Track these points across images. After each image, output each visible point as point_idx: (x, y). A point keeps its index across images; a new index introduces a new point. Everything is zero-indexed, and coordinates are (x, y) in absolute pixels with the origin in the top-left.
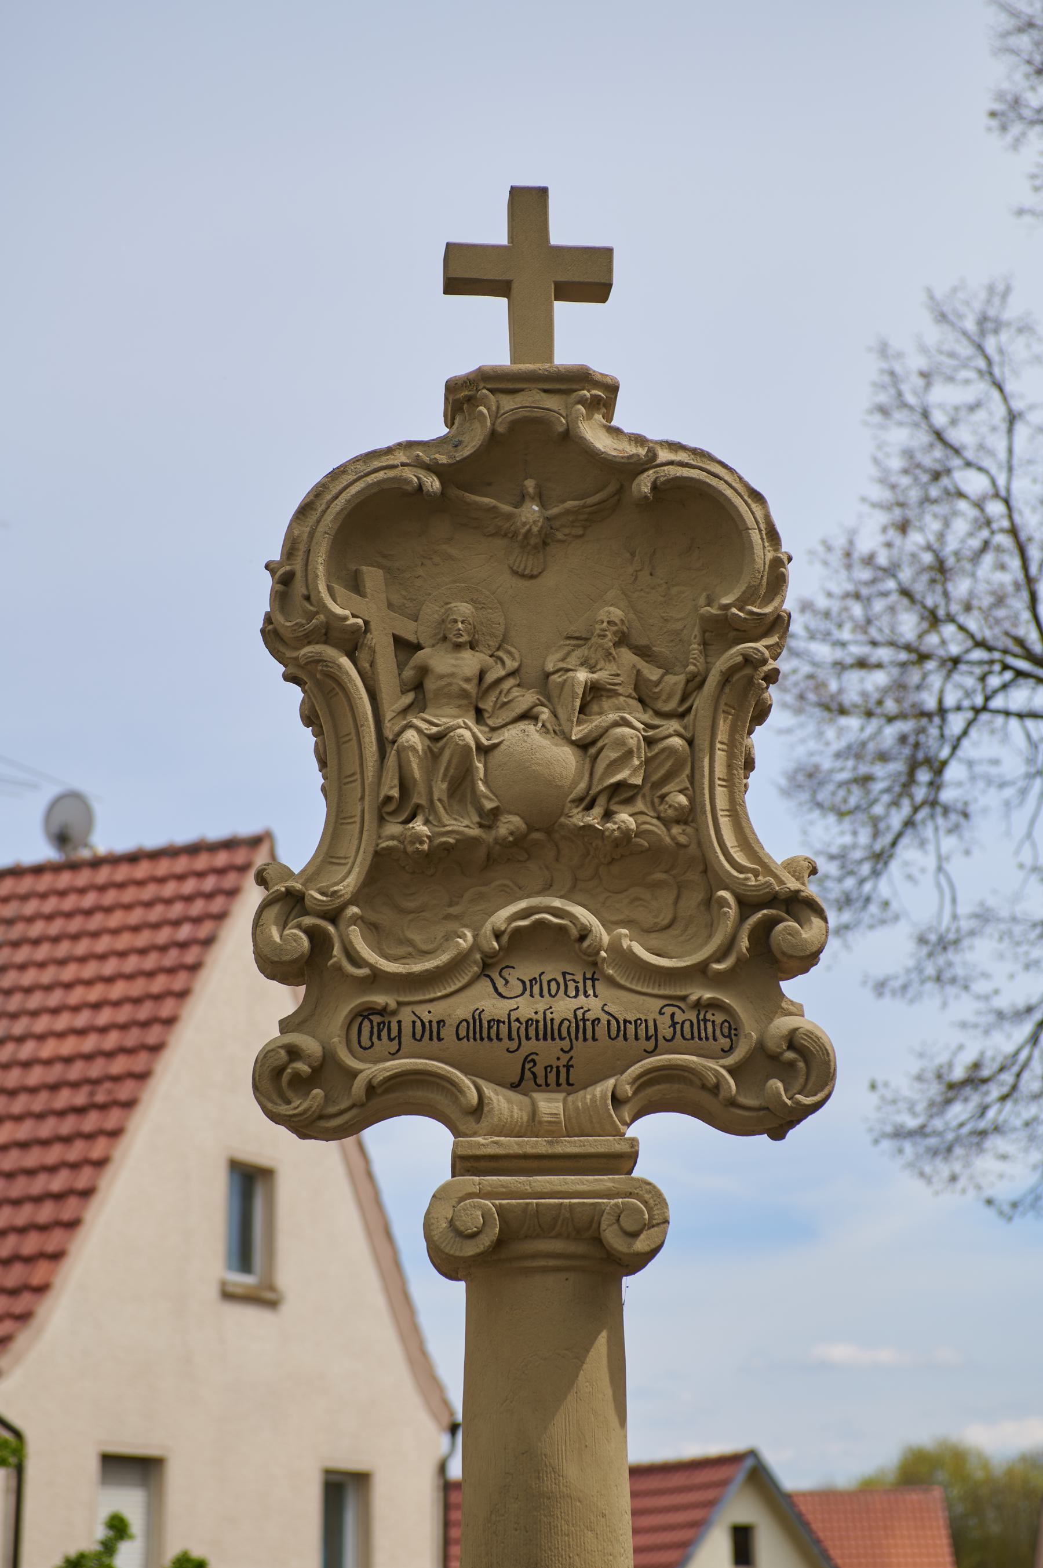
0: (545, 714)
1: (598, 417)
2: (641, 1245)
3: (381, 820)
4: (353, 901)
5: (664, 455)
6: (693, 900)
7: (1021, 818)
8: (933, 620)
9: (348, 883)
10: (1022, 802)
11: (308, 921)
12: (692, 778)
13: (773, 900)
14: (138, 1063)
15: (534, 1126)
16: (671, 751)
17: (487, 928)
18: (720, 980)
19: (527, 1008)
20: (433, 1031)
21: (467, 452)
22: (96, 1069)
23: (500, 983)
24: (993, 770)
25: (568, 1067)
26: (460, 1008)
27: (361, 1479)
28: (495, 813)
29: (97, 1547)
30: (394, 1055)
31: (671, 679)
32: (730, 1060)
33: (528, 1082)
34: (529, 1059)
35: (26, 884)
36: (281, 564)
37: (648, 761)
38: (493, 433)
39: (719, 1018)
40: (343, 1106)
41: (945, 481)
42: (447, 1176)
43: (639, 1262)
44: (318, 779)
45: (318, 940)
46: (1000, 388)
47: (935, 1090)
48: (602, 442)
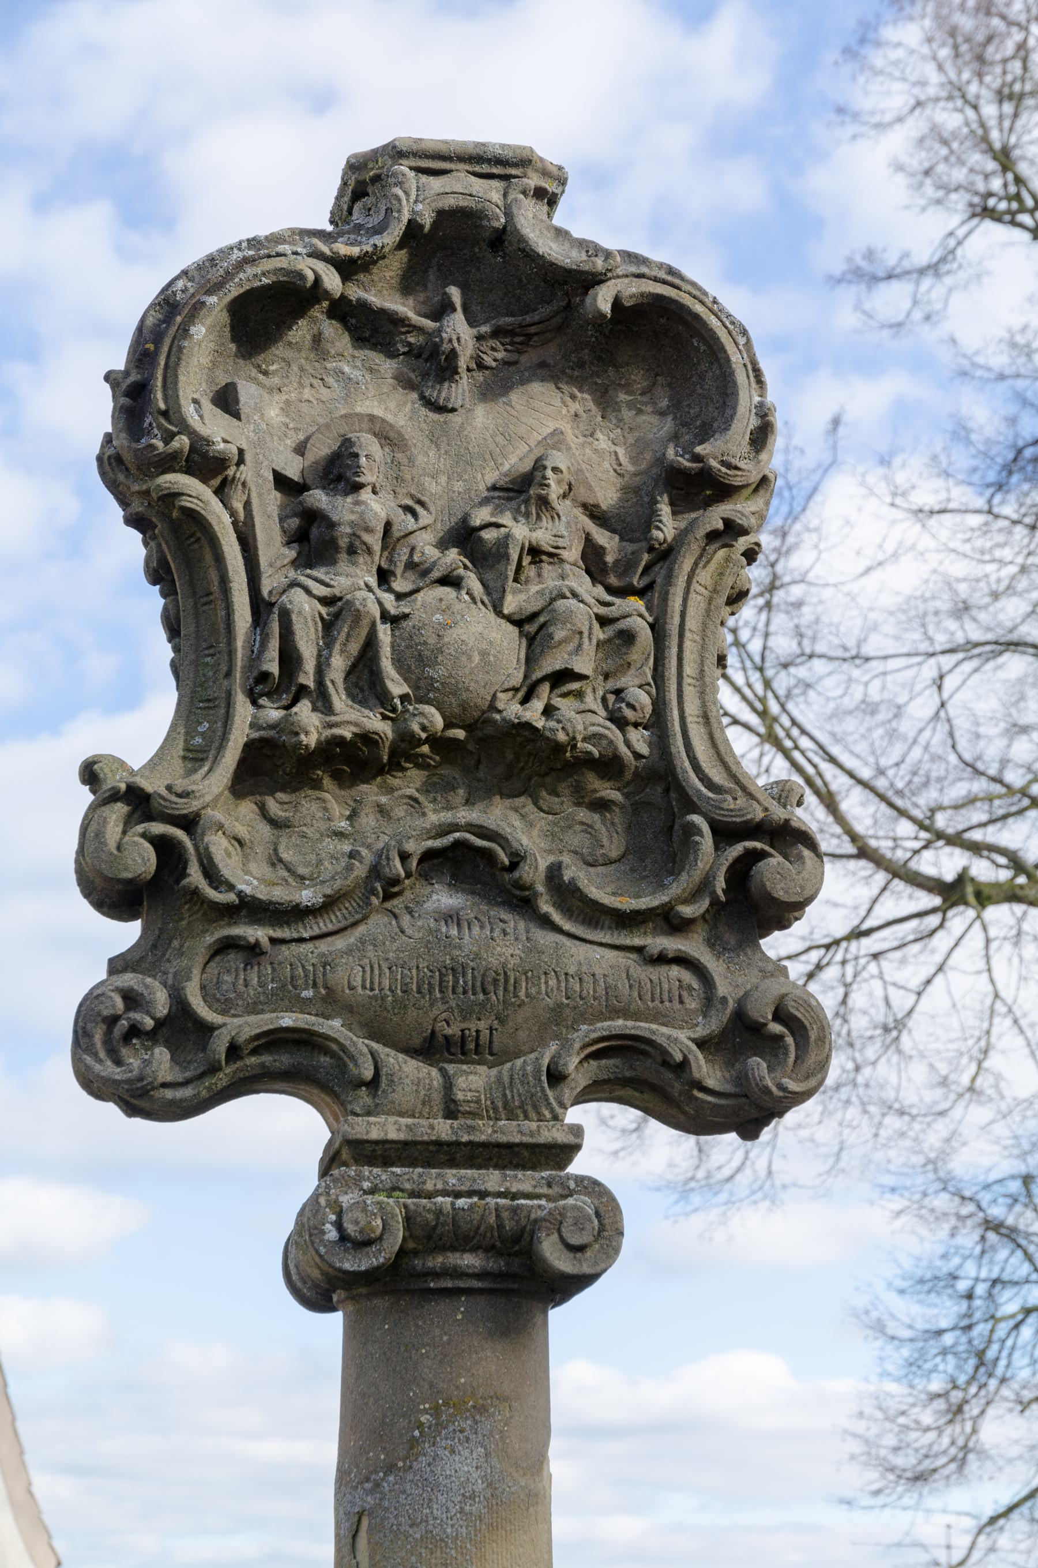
11: (158, 828)
36: (126, 373)
44: (166, 652)
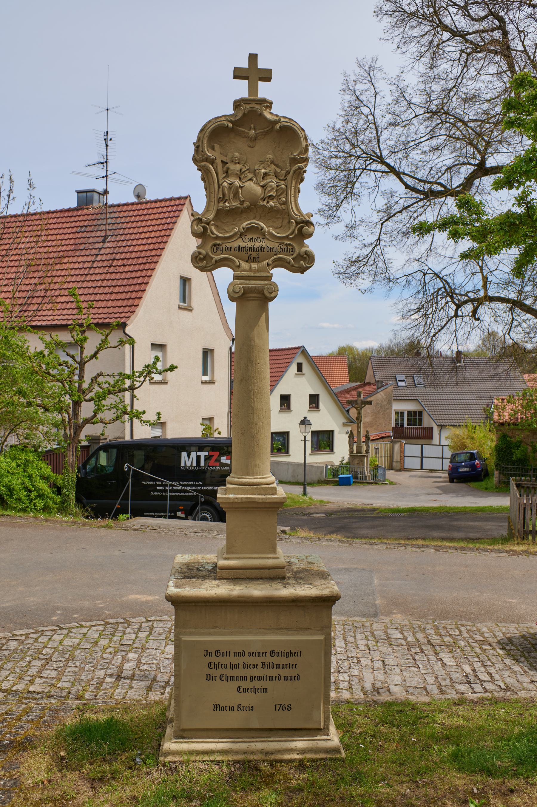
0: (255, 179)
1: (268, 110)
2: (272, 295)
3: (219, 202)
4: (212, 220)
5: (282, 120)
6: (286, 221)
7: (373, 196)
8: (354, 146)
9: (211, 217)
10: (373, 193)
11: (203, 225)
12: (286, 194)
13: (303, 222)
14: (158, 252)
15: (251, 270)
16: (282, 188)
17: (241, 227)
18: (291, 239)
19: (250, 244)
20: (229, 249)
21: (238, 118)
22: (148, 254)
23: (244, 239)
24: (366, 185)
25: (258, 257)
26: (235, 244)
27: (212, 351)
28: (243, 201)
29: (152, 363)
30: (221, 254)
31: (282, 172)
32: (293, 257)
33: (249, 261)
34: (250, 256)
35: (130, 208)
36: (196, 143)
37: (277, 190)
38: (244, 113)
39: (291, 248)
40: (210, 265)
41: (358, 109)
42: (232, 280)
43: (272, 299)
45: (205, 229)
46: (374, 86)
47: (348, 263)
48: (269, 116)
